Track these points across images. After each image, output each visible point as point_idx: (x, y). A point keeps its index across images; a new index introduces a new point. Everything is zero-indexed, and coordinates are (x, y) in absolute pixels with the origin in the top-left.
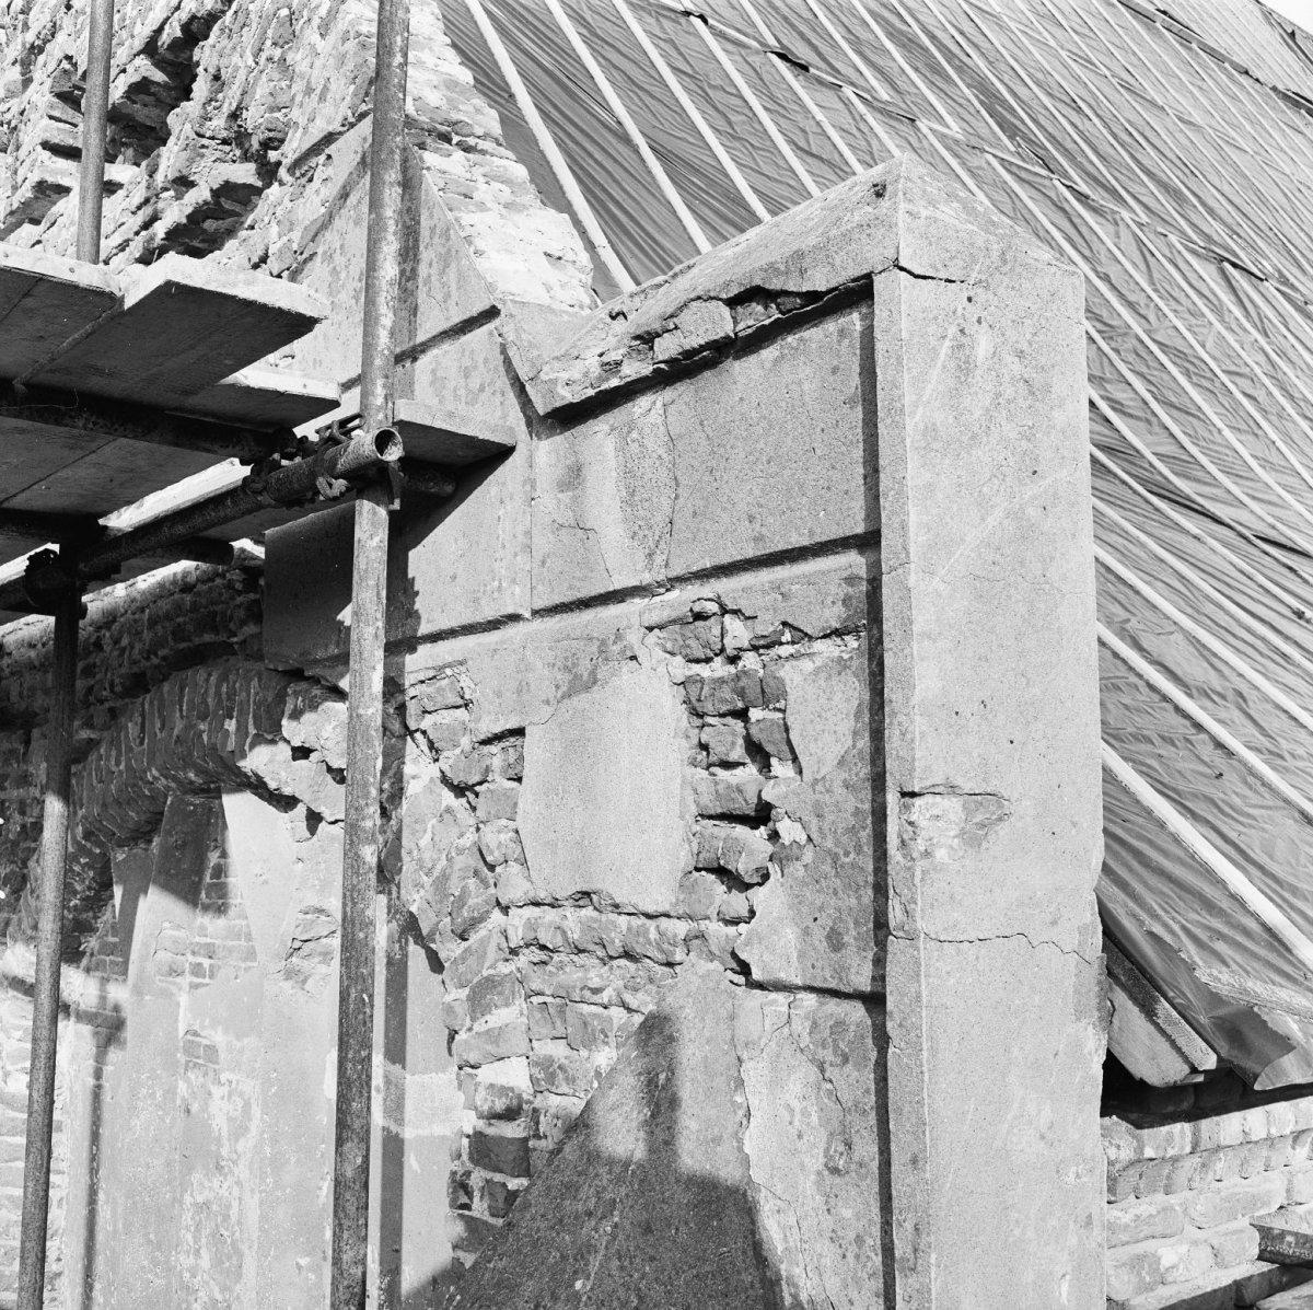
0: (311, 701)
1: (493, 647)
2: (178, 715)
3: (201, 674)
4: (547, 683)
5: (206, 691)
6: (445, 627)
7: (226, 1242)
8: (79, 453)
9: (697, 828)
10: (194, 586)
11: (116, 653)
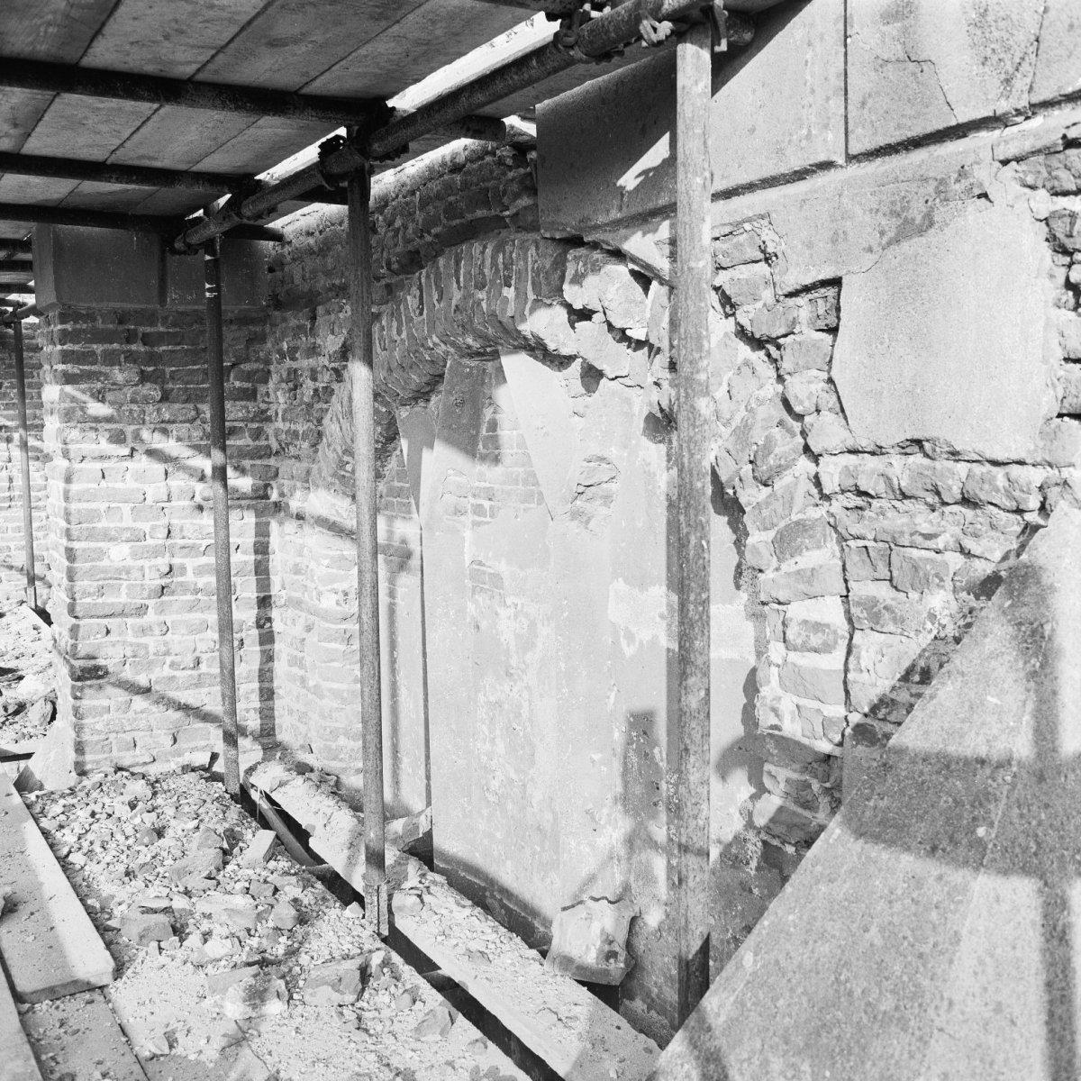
0: (593, 265)
1: (801, 197)
2: (455, 285)
3: (477, 247)
4: (870, 230)
5: (483, 262)
6: (744, 182)
7: (518, 735)
8: (384, 24)
9: (1061, 373)
10: (464, 166)
11: (390, 234)
